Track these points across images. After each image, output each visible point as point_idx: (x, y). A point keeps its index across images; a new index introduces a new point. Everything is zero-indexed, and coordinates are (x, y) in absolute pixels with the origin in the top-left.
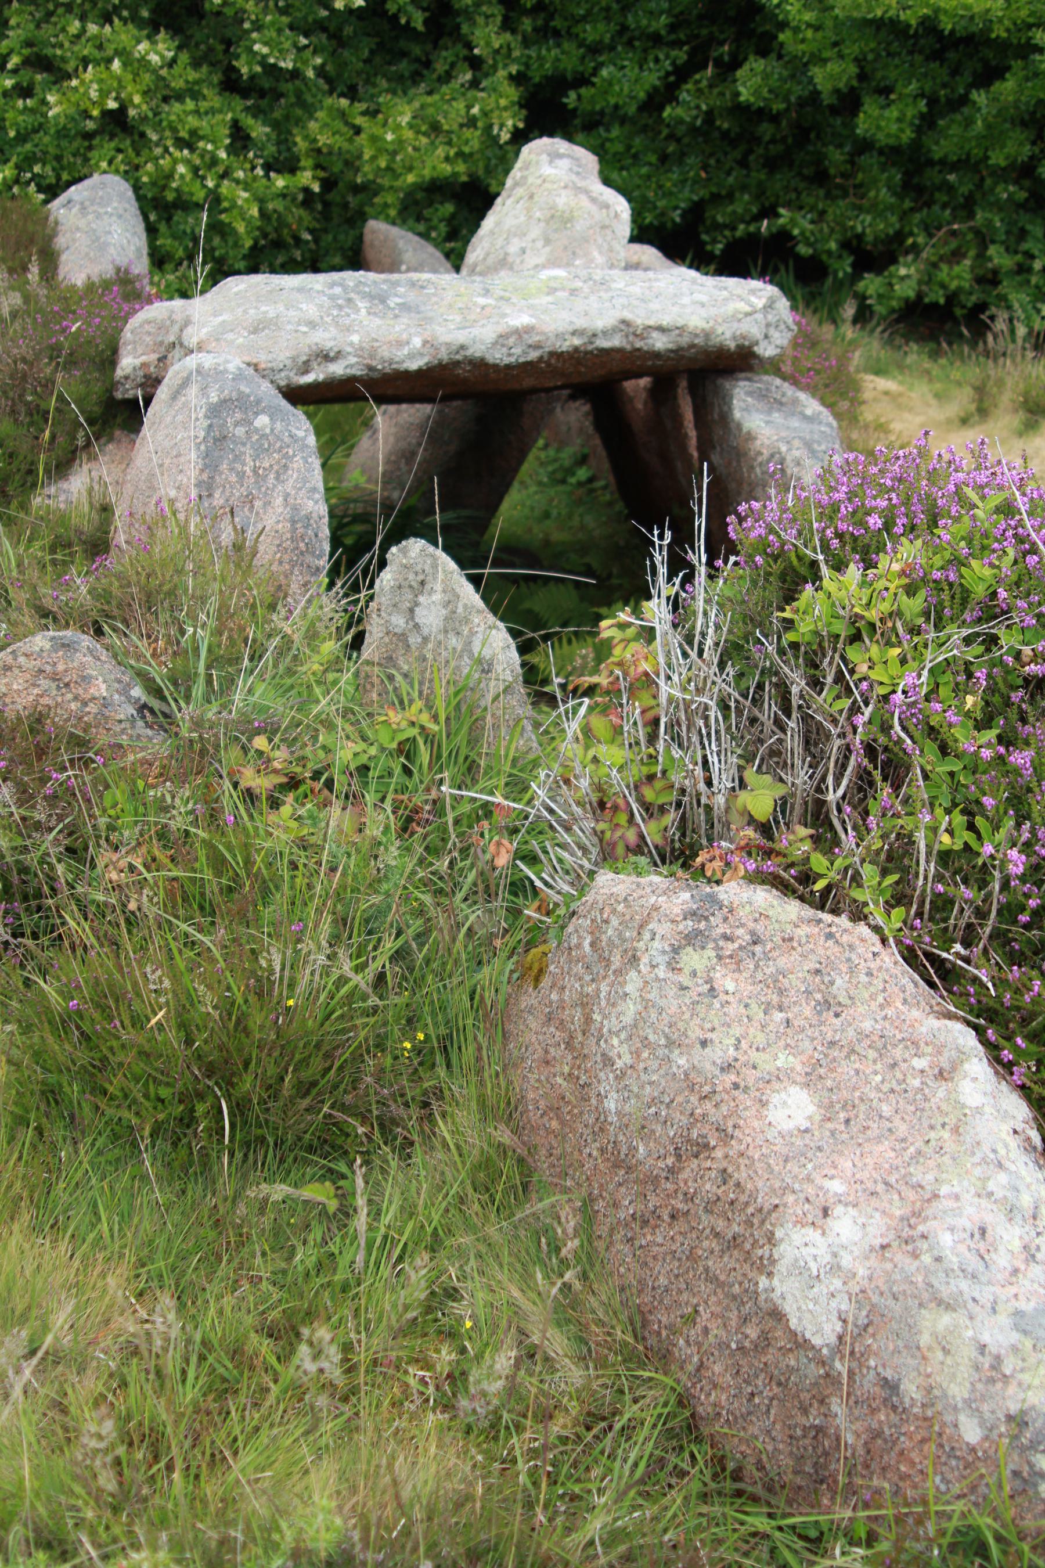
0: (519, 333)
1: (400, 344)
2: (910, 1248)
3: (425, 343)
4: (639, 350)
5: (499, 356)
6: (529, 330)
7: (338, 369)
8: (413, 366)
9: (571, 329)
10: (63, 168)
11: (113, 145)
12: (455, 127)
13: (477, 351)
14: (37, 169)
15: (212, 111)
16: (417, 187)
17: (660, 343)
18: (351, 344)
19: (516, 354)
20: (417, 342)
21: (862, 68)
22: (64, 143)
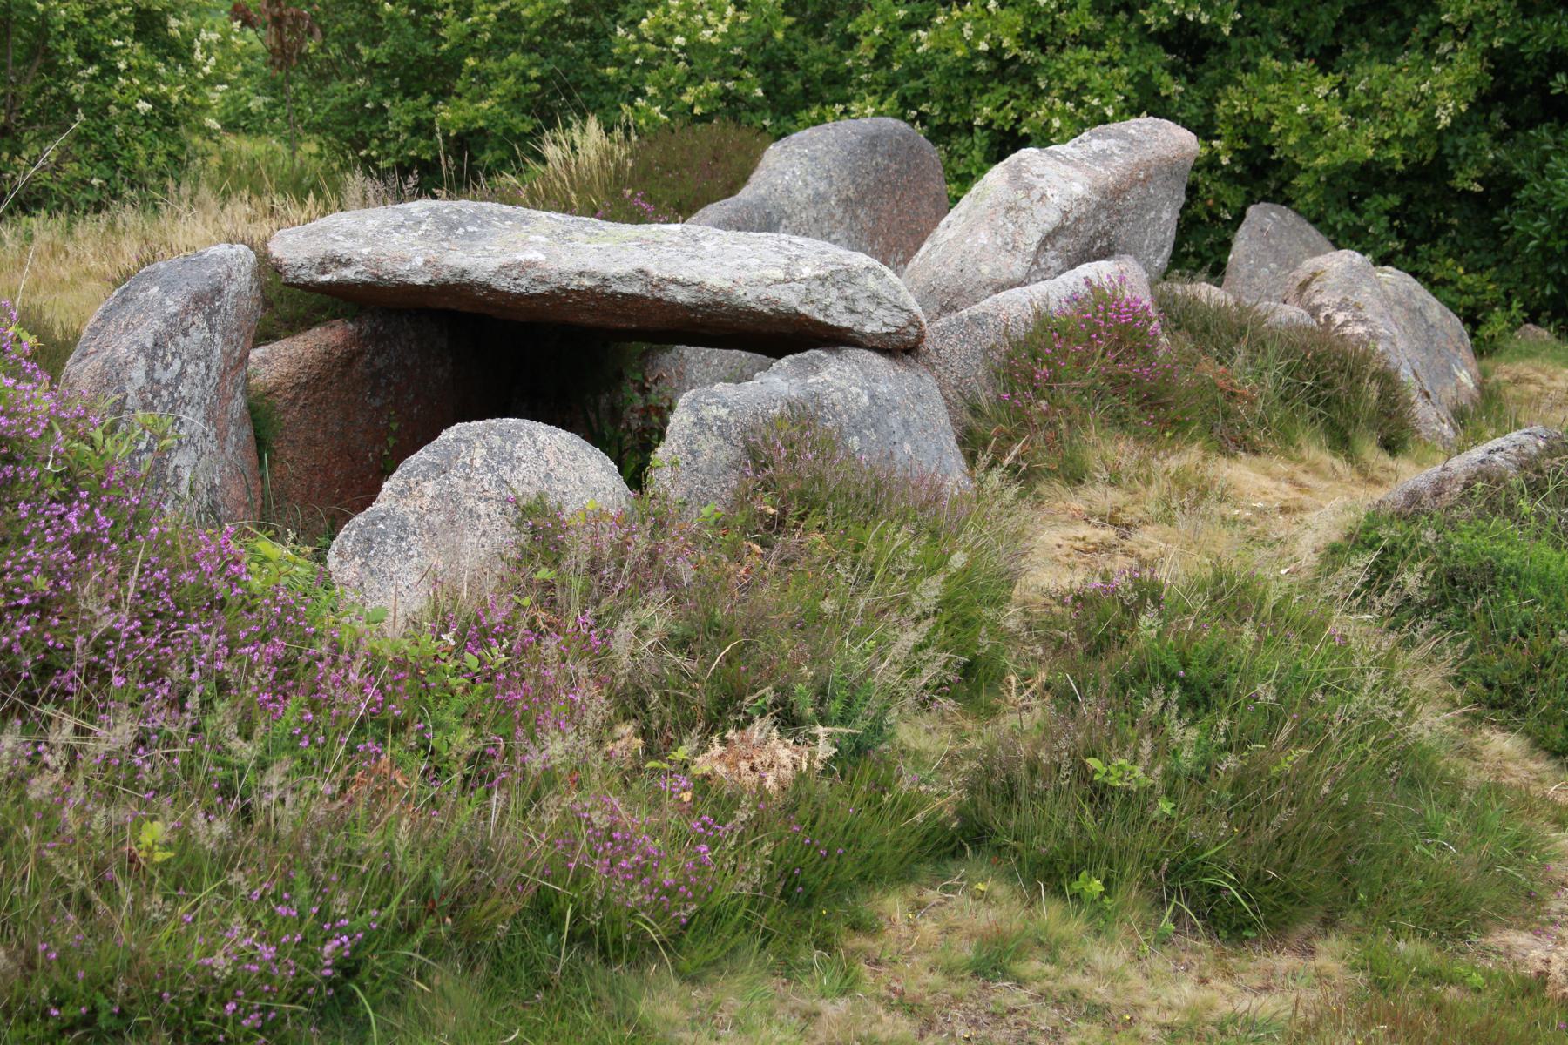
0: (524, 267)
1: (404, 260)
2: (28, 973)
3: (426, 263)
4: (660, 299)
5: (502, 284)
6: (532, 264)
7: (349, 274)
8: (420, 281)
9: (577, 270)
10: (954, 109)
11: (1007, 89)
12: (1399, 104)
13: (481, 276)
14: (924, 108)
15: (1111, 63)
16: (1346, 169)
17: (682, 296)
18: (360, 255)
19: (523, 285)
20: (419, 261)
21: (1082, 43)
22: (954, 84)
